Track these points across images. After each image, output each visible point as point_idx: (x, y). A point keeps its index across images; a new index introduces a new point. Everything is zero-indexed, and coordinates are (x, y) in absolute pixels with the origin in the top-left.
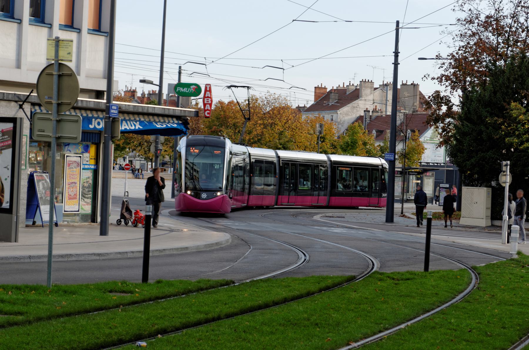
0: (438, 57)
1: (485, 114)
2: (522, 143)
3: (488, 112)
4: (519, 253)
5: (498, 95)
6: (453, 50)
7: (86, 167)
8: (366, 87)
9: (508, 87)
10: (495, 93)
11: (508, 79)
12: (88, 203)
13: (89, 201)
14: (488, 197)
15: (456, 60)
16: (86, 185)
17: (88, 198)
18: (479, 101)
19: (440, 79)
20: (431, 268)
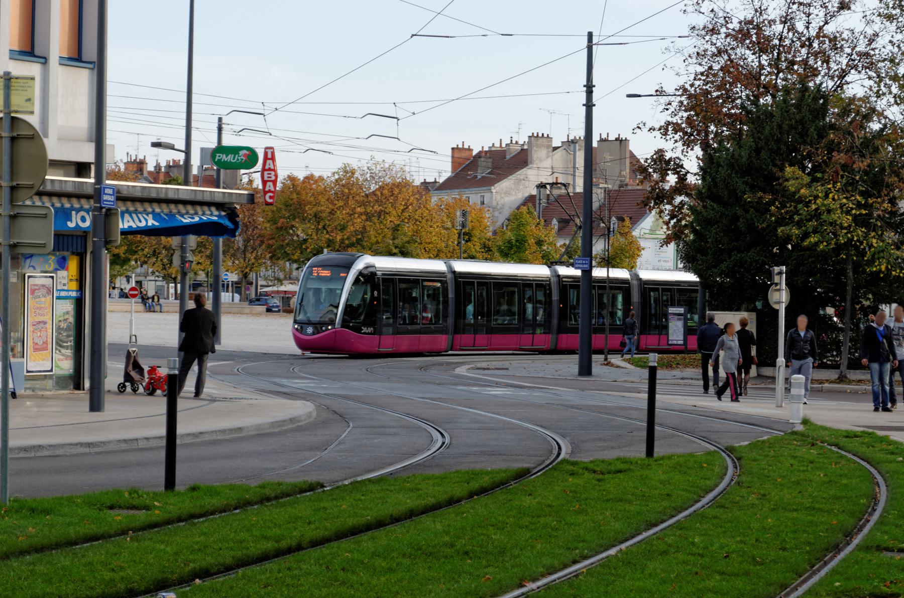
0: (660, 93)
1: (742, 187)
2: (806, 235)
3: (746, 183)
4: (805, 422)
5: (764, 155)
6: (685, 80)
7: (63, 294)
8: (538, 146)
10: (758, 151)
11: (780, 127)
12: (67, 357)
13: (69, 352)
15: (690, 97)
16: (63, 325)
17: (67, 347)
18: (731, 166)
19: (664, 130)
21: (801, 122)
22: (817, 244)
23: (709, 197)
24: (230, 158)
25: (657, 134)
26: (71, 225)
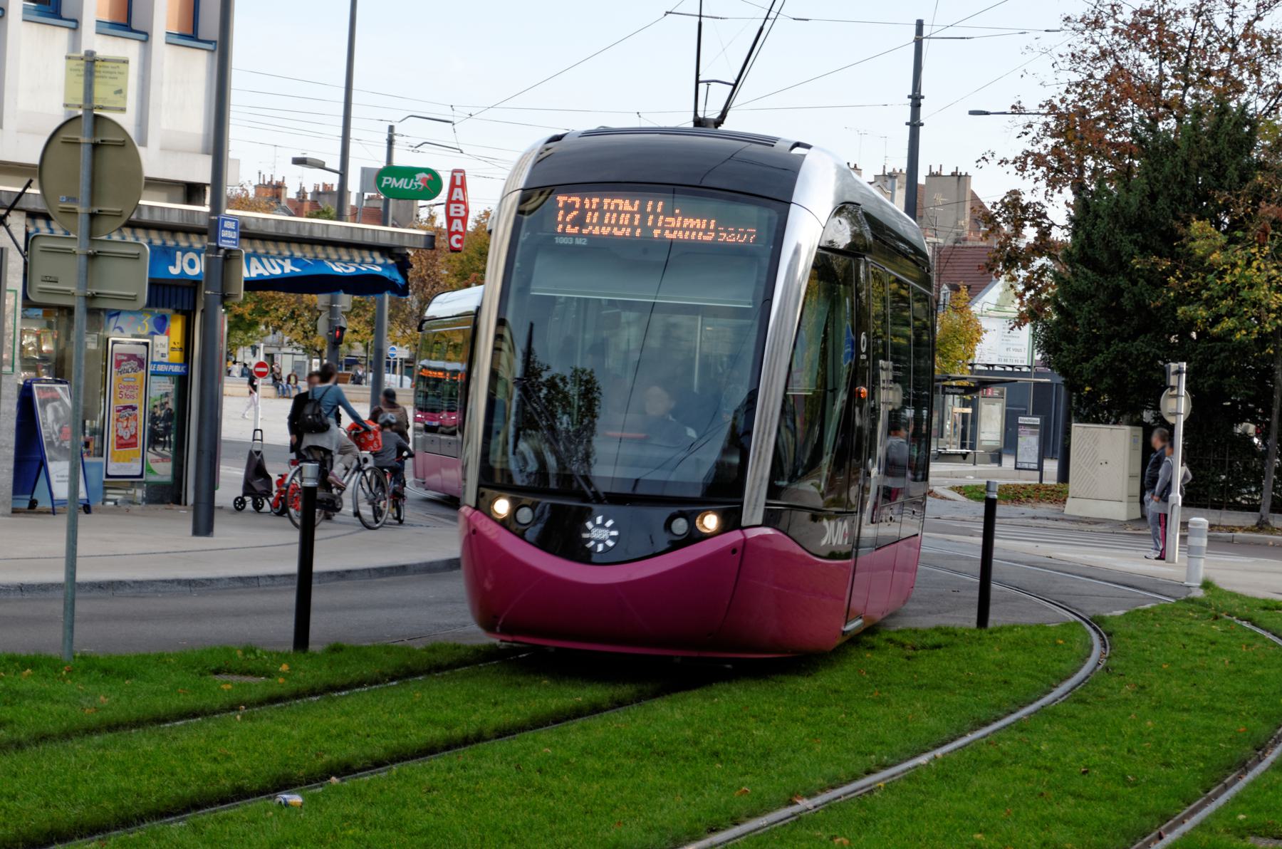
0: (1017, 110)
1: (1129, 247)
2: (1217, 319)
3: (1135, 242)
4: (1207, 585)
5: (1162, 202)
6: (1054, 92)
9: (1183, 183)
10: (1153, 197)
11: (1186, 163)
12: (164, 458)
13: (167, 451)
14: (1133, 449)
16: (160, 413)
17: (164, 444)
18: (1115, 217)
20: (994, 619)
21: (1217, 157)
22: (1232, 331)
23: (1081, 261)
24: (402, 184)
25: (1011, 168)
26: (174, 271)
